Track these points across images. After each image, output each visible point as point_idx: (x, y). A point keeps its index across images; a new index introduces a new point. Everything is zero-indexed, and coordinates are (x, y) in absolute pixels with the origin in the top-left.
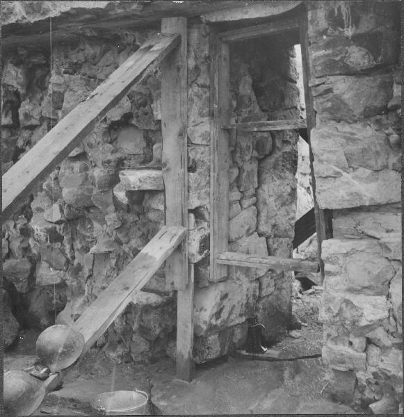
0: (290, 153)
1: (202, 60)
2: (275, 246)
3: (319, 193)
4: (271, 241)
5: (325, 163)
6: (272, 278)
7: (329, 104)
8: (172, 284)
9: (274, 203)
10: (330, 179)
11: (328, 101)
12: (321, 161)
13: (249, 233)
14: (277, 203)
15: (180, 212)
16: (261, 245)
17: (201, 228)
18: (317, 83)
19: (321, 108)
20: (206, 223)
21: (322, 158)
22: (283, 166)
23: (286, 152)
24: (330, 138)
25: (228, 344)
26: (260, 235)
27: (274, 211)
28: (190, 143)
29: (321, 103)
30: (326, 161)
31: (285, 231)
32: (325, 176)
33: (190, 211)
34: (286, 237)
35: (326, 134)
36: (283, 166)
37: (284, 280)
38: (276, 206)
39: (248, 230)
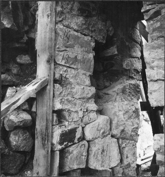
0: (134, 85)
1: (68, 10)
2: (124, 145)
3: (151, 93)
4: (120, 141)
5: (155, 68)
6: (121, 167)
7: (158, 24)
8: (38, 173)
9: (122, 116)
10: (159, 82)
11: (157, 21)
12: (152, 68)
13: (104, 135)
14: (125, 116)
15: (45, 118)
16: (113, 144)
17: (63, 125)
18: (148, 8)
19: (151, 29)
20: (67, 122)
21: (153, 64)
22: (129, 92)
23: (131, 84)
24: (160, 48)
25: (13, 75)
26: (113, 136)
27: (123, 121)
28: (56, 64)
29: (152, 25)
30: (156, 67)
31: (131, 135)
32: (156, 79)
33: (54, 112)
34: (132, 140)
35: (156, 45)
36: (129, 92)
37: (130, 169)
38: (124, 118)
39: (103, 133)
